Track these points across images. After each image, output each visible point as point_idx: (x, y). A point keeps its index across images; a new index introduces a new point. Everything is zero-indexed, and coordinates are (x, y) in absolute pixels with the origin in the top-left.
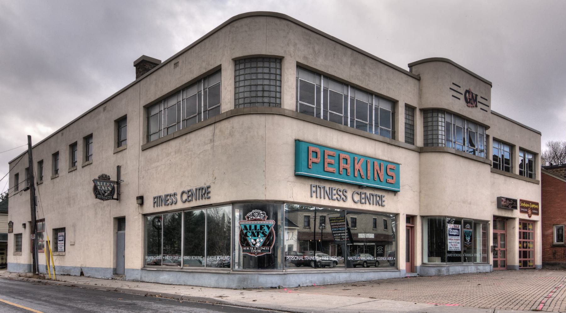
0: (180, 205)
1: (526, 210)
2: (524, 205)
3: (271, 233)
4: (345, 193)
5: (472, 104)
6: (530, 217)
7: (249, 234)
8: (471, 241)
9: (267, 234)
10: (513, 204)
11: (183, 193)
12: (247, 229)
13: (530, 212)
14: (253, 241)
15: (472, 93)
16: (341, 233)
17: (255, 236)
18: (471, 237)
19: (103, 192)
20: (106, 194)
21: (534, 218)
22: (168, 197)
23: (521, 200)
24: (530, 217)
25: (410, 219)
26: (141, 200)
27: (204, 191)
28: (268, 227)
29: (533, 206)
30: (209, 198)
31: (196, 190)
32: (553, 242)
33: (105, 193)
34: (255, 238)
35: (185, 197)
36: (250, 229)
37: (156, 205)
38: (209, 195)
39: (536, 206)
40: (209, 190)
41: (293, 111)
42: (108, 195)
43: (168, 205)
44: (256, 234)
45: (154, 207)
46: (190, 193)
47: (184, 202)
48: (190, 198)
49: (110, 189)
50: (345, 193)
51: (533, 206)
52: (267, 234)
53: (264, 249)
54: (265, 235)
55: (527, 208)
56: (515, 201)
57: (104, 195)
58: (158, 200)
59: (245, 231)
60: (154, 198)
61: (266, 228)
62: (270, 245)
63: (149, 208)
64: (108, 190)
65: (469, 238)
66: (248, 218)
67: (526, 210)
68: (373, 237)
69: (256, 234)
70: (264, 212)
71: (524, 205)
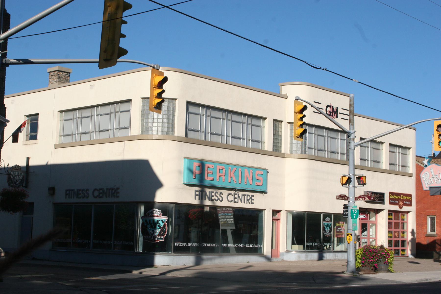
0: (91, 199)
1: (397, 202)
2: (395, 197)
3: (164, 226)
4: (221, 195)
5: (332, 116)
6: (401, 208)
7: (149, 226)
8: (330, 231)
9: (162, 226)
10: (380, 197)
11: (95, 190)
12: (147, 223)
13: (401, 203)
14: (151, 231)
15: (333, 107)
16: (227, 218)
17: (152, 228)
18: (331, 228)
19: (15, 181)
20: (18, 183)
21: (405, 208)
22: (81, 192)
23: (391, 194)
24: (401, 208)
25: (276, 212)
26: (52, 191)
27: (113, 191)
28: (162, 221)
29: (405, 198)
30: (118, 197)
31: (107, 189)
32: (427, 232)
33: (17, 181)
34: (153, 229)
35: (96, 193)
36: (150, 223)
37: (67, 196)
38: (118, 195)
39: (409, 198)
40: (118, 191)
41: (183, 137)
42: (19, 183)
43: (80, 198)
44: (154, 226)
45: (66, 198)
46: (101, 191)
47: (96, 197)
48: (101, 195)
49: (21, 178)
50: (221, 195)
51: (405, 198)
52: (162, 226)
53: (159, 237)
54: (160, 228)
55: (398, 200)
56: (382, 195)
57: (15, 183)
58: (69, 193)
59: (146, 224)
60: (67, 191)
61: (161, 222)
62: (163, 235)
63: (60, 198)
64: (19, 179)
65: (329, 230)
66: (148, 214)
67: (397, 202)
68: (134, 271)
69: (154, 226)
70: (160, 211)
71: (395, 197)
